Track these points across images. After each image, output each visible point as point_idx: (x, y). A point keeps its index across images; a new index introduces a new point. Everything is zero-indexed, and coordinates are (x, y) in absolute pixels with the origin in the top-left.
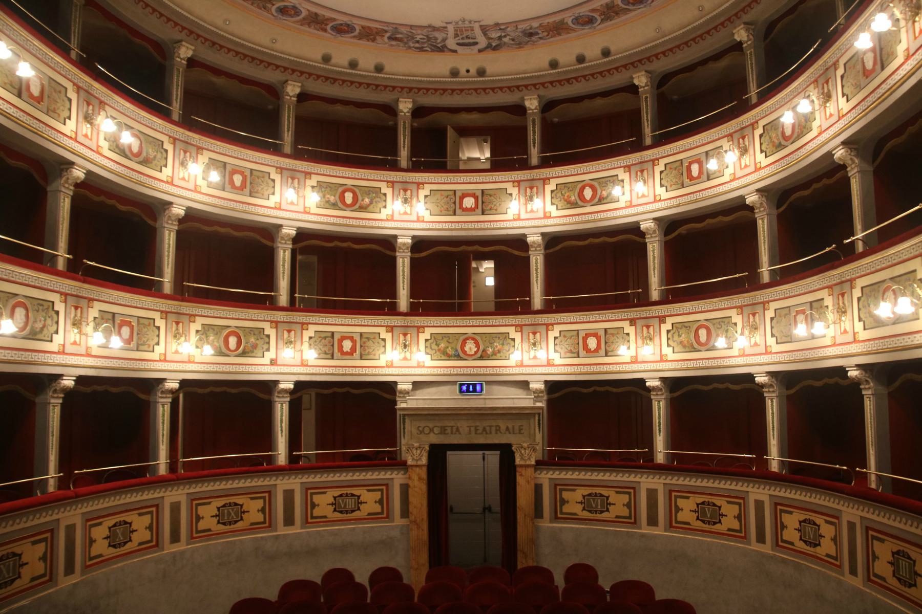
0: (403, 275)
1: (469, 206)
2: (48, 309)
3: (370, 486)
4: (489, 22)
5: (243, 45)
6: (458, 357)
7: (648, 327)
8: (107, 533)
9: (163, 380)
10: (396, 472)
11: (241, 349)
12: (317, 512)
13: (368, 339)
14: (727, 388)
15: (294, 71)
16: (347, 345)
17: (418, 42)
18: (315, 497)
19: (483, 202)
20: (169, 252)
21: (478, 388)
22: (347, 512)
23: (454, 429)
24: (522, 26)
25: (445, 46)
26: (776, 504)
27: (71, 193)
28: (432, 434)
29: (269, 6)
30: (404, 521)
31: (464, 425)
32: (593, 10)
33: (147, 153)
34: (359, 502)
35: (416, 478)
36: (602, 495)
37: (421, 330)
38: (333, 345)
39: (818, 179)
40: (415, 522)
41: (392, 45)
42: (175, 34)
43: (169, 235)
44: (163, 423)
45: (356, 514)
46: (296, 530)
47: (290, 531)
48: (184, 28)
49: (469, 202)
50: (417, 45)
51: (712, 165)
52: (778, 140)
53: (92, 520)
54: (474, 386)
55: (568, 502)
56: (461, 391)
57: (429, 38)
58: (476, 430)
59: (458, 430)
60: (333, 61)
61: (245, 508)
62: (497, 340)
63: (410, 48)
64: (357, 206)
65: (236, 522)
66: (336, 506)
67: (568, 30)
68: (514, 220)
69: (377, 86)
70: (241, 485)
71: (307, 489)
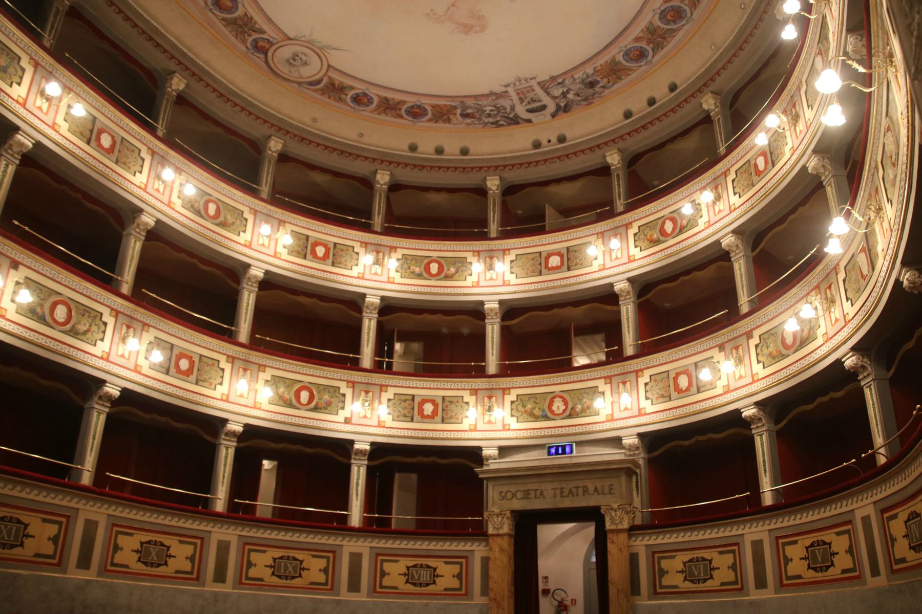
0: (493, 341)
1: (554, 265)
3: (449, 558)
4: (544, 77)
5: (331, 139)
6: (546, 418)
7: (737, 348)
10: (477, 544)
11: (313, 404)
12: (386, 581)
13: (451, 402)
14: (832, 399)
15: (382, 161)
16: (428, 408)
17: (489, 115)
18: (385, 564)
19: (568, 259)
20: (247, 310)
21: (568, 449)
22: (421, 585)
23: (538, 492)
24: (579, 75)
25: (516, 116)
28: (514, 500)
29: (343, 96)
30: (484, 600)
31: (548, 487)
32: (637, 39)
33: (225, 218)
34: (435, 575)
35: (496, 549)
36: (704, 559)
37: (507, 392)
38: (413, 408)
40: (495, 599)
41: (468, 124)
42: (265, 130)
43: (249, 295)
44: (225, 465)
45: (431, 588)
46: (361, 597)
47: (218, 588)
48: (273, 125)
49: (555, 261)
50: (491, 120)
54: (564, 447)
55: (667, 572)
56: (549, 454)
57: (498, 109)
58: (562, 492)
59: (542, 494)
60: (420, 149)
61: (304, 565)
62: (585, 395)
63: (485, 124)
64: (442, 275)
65: (293, 578)
66: (408, 576)
67: (627, 71)
68: (600, 270)
69: (464, 169)
70: (302, 539)
71: (378, 555)
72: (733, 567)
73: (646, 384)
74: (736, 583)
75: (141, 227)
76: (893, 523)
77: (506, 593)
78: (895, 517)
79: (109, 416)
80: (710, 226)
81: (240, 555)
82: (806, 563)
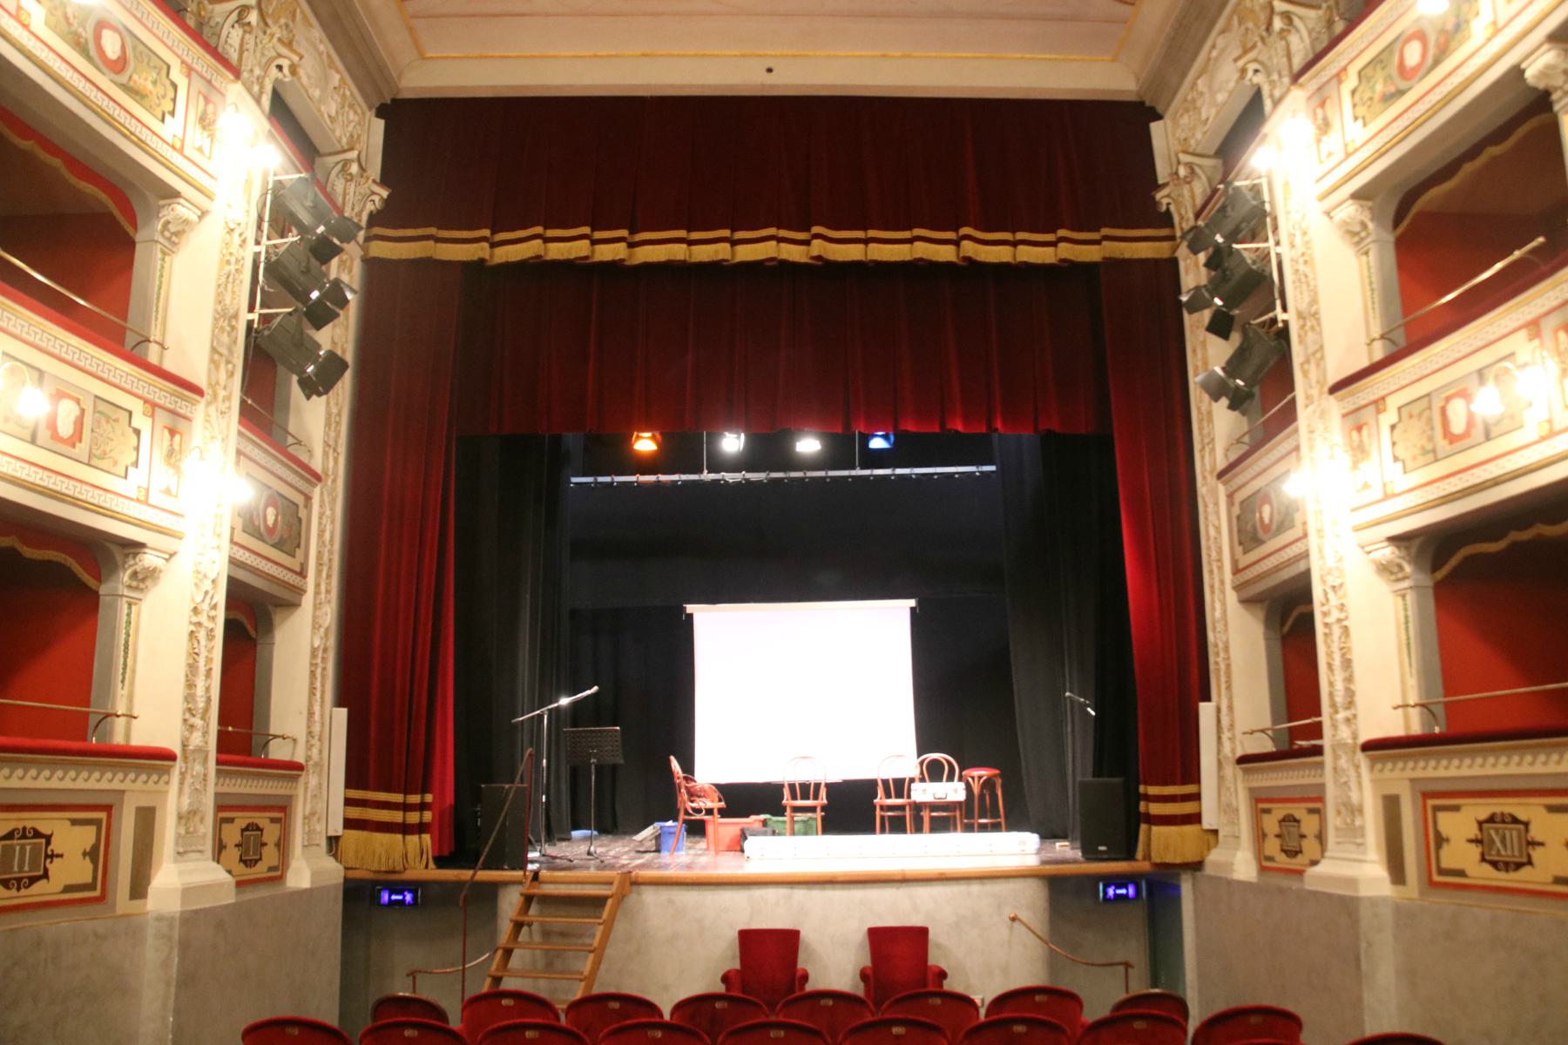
26: (1426, 795)
51: (1486, 403)
73: (1393, 427)
76: (275, 863)
77: (164, 865)
78: (271, 869)
80: (1497, 31)
81: (1421, 824)
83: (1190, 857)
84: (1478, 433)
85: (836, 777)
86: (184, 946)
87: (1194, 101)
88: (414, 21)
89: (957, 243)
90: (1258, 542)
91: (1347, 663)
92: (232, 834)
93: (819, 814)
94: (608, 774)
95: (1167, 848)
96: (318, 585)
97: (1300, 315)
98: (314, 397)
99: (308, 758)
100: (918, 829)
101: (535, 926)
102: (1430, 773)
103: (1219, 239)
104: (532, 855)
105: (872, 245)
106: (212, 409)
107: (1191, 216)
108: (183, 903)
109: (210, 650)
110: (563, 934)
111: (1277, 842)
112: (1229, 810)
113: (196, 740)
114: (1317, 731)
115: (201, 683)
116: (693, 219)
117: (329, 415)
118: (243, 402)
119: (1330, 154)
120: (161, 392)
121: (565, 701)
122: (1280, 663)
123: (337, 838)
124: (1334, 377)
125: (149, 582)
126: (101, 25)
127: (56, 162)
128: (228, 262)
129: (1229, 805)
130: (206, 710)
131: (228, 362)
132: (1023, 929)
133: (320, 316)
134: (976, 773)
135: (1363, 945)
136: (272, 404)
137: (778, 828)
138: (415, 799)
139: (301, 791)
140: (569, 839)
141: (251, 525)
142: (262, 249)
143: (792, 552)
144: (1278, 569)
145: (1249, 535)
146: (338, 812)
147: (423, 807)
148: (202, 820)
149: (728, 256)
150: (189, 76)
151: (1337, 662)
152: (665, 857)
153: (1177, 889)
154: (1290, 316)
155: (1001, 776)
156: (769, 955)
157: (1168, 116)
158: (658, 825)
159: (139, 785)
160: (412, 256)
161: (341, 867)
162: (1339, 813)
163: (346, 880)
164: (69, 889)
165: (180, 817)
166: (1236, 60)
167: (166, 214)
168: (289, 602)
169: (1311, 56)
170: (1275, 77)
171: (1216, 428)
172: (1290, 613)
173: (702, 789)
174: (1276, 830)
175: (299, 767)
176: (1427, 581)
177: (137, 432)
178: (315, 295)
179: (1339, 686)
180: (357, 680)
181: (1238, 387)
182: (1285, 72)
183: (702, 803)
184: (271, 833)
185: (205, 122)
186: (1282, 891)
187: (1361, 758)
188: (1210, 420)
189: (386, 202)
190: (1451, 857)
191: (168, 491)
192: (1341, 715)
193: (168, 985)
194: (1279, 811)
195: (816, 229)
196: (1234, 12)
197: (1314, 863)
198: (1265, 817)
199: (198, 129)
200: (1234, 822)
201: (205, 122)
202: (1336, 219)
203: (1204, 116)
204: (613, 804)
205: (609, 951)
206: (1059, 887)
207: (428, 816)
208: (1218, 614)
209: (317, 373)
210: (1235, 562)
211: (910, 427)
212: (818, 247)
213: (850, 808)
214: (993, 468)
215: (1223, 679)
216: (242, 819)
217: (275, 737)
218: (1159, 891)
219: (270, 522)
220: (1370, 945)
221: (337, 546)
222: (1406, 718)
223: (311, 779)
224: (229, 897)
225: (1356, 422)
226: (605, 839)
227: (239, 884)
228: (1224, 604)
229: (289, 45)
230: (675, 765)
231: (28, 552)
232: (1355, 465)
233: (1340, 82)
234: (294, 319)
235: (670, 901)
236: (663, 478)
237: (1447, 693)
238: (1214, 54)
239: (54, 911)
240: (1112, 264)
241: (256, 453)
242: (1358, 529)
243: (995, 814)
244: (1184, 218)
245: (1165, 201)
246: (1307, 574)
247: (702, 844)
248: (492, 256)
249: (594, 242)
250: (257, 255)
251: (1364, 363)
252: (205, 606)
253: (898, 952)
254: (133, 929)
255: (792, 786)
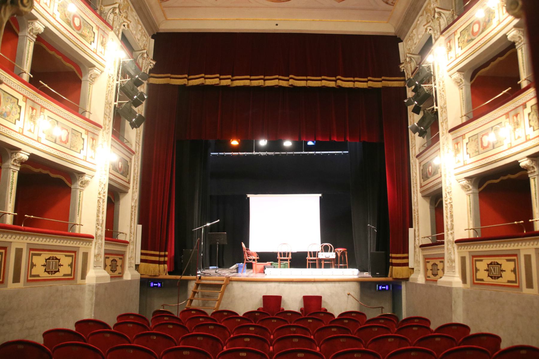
2: (14, 102)
8: (44, 262)
9: (18, 149)
26: (473, 257)
27: (18, 169)
39: (494, 59)
52: (470, 34)
53: (35, 250)
72: (514, 271)
74: (515, 282)
75: (34, 31)
78: (119, 273)
79: (20, 173)
80: (500, 23)
82: (44, 268)
83: (405, 277)
84: (491, 147)
85: (295, 250)
86: (97, 294)
87: (412, 37)
88: (165, 9)
89: (335, 81)
90: (428, 178)
91: (452, 216)
92: (109, 262)
93: (289, 262)
94: (222, 247)
95: (397, 273)
96: (133, 186)
97: (441, 108)
98: (134, 128)
99: (130, 240)
100: (320, 267)
101: (200, 294)
102: (474, 250)
103: (417, 83)
104: (199, 272)
105: (308, 81)
106: (104, 132)
107: (410, 74)
108: (96, 281)
109: (103, 206)
110: (208, 296)
111: (431, 271)
112: (417, 261)
113: (99, 233)
114: (442, 237)
115: (101, 215)
116: (252, 72)
117: (137, 133)
118: (113, 130)
119: (451, 58)
120: (90, 127)
121: (208, 224)
122: (434, 216)
123: (138, 265)
124: (450, 128)
125: (86, 185)
126: (74, 16)
127: (60, 57)
128: (109, 87)
129: (417, 260)
130: (102, 224)
131: (109, 117)
132: (352, 298)
133: (137, 103)
134: (339, 250)
135: (453, 302)
136: (119, 129)
137: (275, 265)
138: (162, 253)
139: (128, 250)
140: (209, 269)
141: (115, 168)
142: (119, 82)
143: (283, 178)
144: (433, 186)
145: (425, 176)
146: (139, 257)
147: (165, 256)
148: (101, 257)
149: (263, 84)
150: (98, 30)
151: (449, 216)
152: (240, 274)
153: (401, 286)
154: (438, 108)
155: (347, 251)
156: (272, 302)
157: (404, 42)
158: (237, 264)
159: (83, 246)
160: (163, 83)
161: (139, 274)
162: (448, 262)
163: (141, 278)
164: (65, 275)
165: (95, 256)
166: (424, 26)
167: (91, 72)
168: (124, 191)
169: (447, 26)
170: (436, 32)
171: (416, 142)
172: (436, 199)
173: (252, 253)
174: (431, 268)
175: (127, 243)
176: (477, 191)
177: (83, 139)
178: (135, 97)
179: (449, 223)
180: (144, 217)
181: (421, 129)
182: (439, 31)
183: (251, 257)
184: (119, 263)
185: (103, 44)
186: (431, 286)
187: (455, 245)
188: (415, 139)
189: (155, 66)
190: (480, 275)
191: (92, 157)
192: (449, 232)
193: (92, 305)
194: (432, 262)
195: (291, 76)
196: (425, 10)
197: (441, 278)
198: (428, 264)
199: (101, 46)
200: (418, 266)
201: (103, 44)
202: (453, 78)
203: (415, 42)
204: (223, 257)
205: (222, 301)
206: (363, 284)
207: (166, 259)
208: (415, 200)
209: (136, 121)
210: (421, 184)
211: (320, 140)
212: (291, 82)
213: (299, 260)
214: (347, 152)
215: (416, 221)
216: (112, 258)
217: (121, 233)
218: (395, 286)
219: (120, 167)
220: (455, 302)
221: (139, 174)
222: (469, 233)
223: (131, 247)
224: (108, 281)
225: (456, 140)
226: (220, 269)
227: (111, 277)
228: (417, 197)
229: (126, 18)
230: (243, 245)
231: (52, 175)
232: (456, 155)
233: (455, 35)
234: (129, 104)
235: (242, 286)
236: (240, 153)
237: (482, 226)
238: (418, 22)
239: (61, 281)
240: (385, 88)
241: (116, 146)
242: (456, 175)
243: (345, 263)
244: (409, 75)
245: (402, 68)
246: (441, 189)
247: (252, 271)
248: (188, 83)
249: (221, 79)
250: (117, 84)
251: (460, 123)
252: (102, 192)
253: (312, 303)
254: (82, 288)
255: (280, 253)
